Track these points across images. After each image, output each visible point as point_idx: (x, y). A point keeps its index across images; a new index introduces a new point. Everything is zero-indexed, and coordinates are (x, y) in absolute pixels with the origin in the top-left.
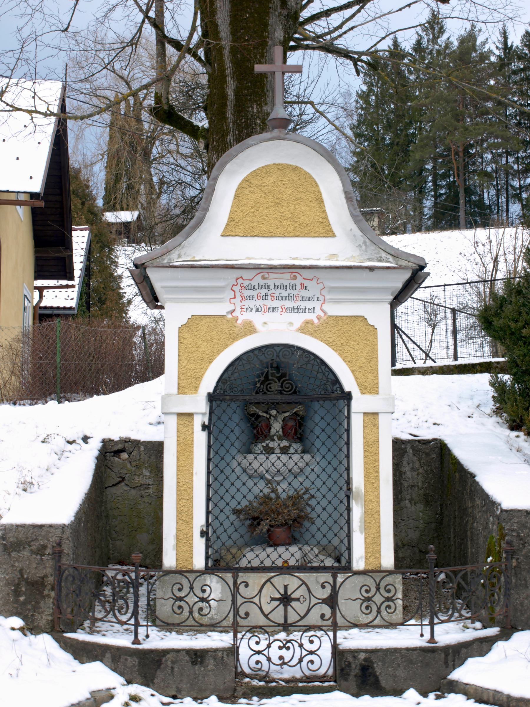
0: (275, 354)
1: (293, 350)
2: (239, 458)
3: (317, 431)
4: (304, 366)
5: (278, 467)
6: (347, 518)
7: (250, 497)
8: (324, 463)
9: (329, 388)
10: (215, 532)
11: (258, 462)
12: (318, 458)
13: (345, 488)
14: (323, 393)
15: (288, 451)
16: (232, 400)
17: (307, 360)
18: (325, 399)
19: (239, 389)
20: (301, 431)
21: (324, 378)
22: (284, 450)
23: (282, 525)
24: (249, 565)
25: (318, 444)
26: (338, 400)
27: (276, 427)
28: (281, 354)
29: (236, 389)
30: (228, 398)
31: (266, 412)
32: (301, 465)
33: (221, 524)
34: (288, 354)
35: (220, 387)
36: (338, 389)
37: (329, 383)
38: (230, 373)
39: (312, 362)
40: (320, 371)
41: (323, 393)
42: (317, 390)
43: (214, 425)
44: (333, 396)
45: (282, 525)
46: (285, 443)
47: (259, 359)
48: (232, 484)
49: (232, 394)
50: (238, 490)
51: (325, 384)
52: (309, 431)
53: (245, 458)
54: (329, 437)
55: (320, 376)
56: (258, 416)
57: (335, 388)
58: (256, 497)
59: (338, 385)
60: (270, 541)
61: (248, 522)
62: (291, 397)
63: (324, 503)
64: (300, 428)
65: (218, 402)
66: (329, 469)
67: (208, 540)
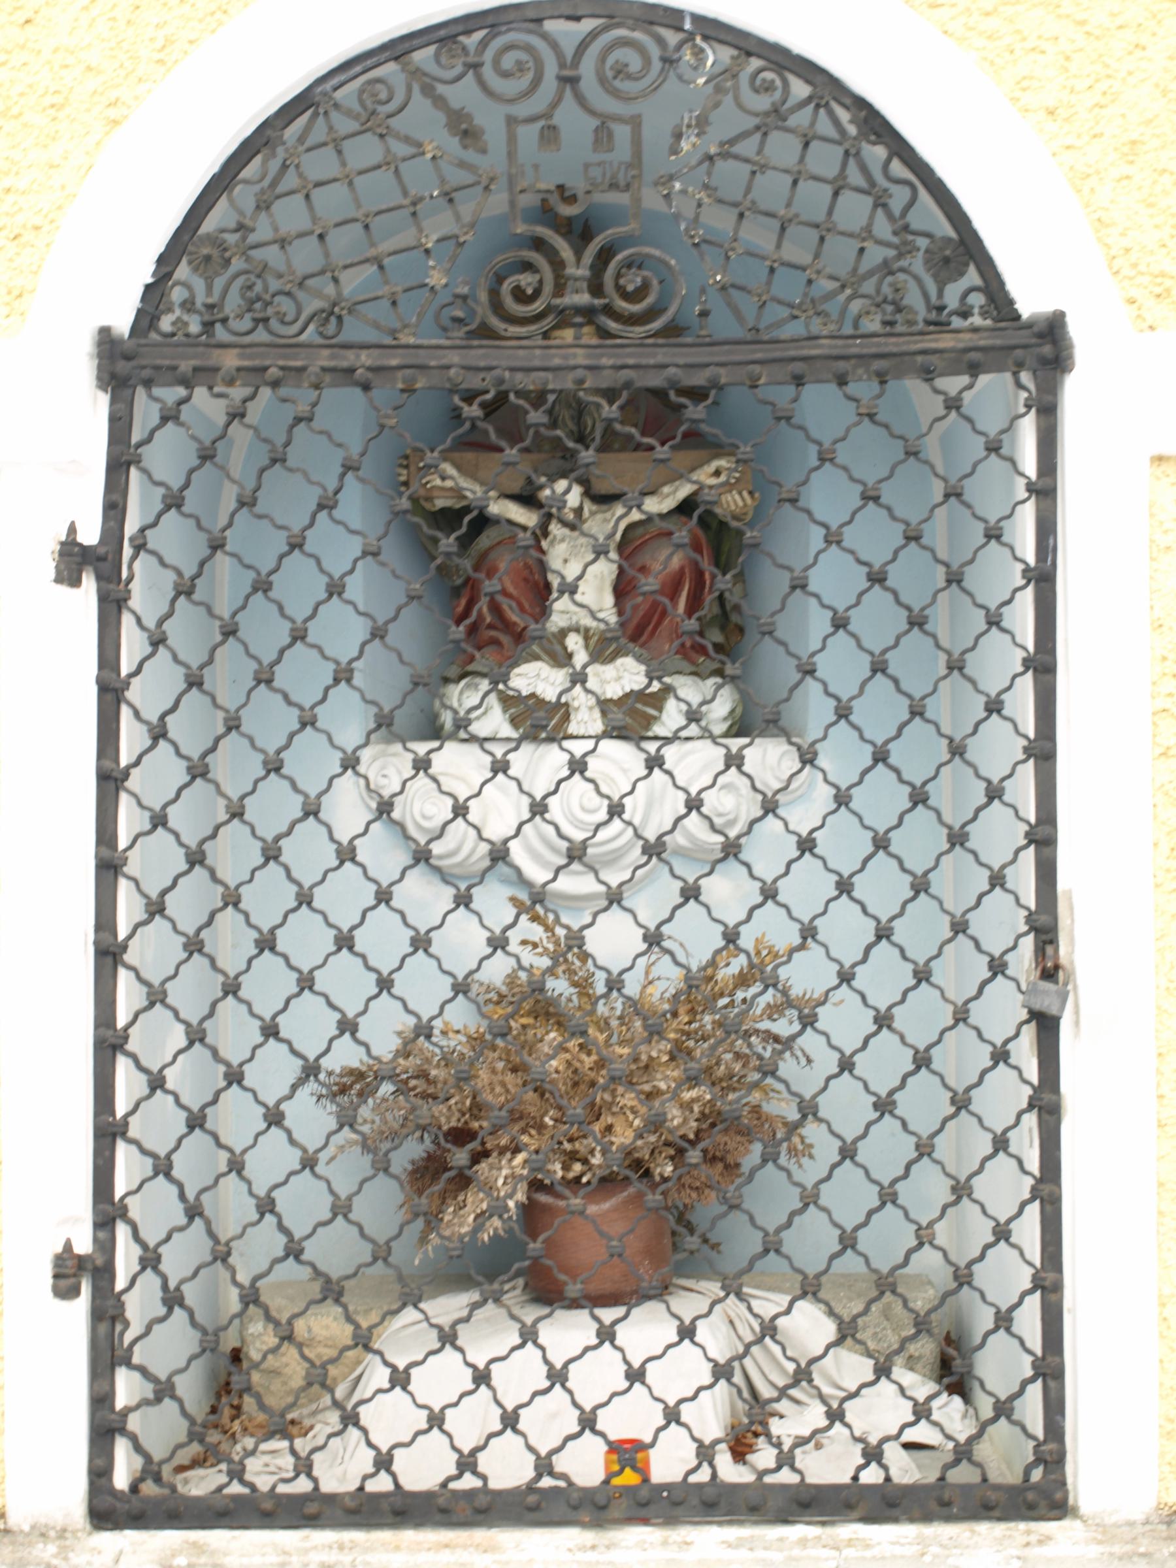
0: (551, 69)
1: (672, 38)
2: (388, 766)
3: (835, 579)
4: (742, 148)
5: (586, 824)
6: (1033, 1163)
7: (424, 988)
8: (881, 798)
9: (913, 299)
10: (150, 1260)
11: (478, 785)
12: (842, 756)
13: (1023, 960)
14: (872, 324)
15: (649, 721)
16: (255, 374)
17: (762, 103)
18: (888, 367)
19: (312, 305)
20: (724, 582)
21: (883, 228)
22: (629, 720)
23: (608, 1182)
24: (382, 1484)
25: (841, 665)
26: (974, 370)
27: (587, 586)
28: (587, 68)
29: (286, 305)
30: (230, 360)
31: (528, 499)
32: (731, 803)
33: (194, 1212)
34: (635, 63)
35: (177, 295)
36: (977, 300)
37: (917, 264)
38: (244, 195)
39: (801, 119)
40: (855, 177)
41: (872, 324)
42: (833, 307)
43: (140, 547)
44: (946, 342)
45: (608, 1182)
46: (625, 676)
47: (440, 102)
48: (266, 943)
49: (261, 335)
50: (306, 983)
51: (887, 269)
52: (785, 579)
53: (422, 765)
54: (917, 622)
55: (854, 210)
56: (483, 521)
57: (952, 296)
58: (461, 988)
59: (972, 277)
60: (534, 1270)
61: (412, 1150)
62: (661, 356)
63: (885, 1063)
64: (722, 563)
65: (171, 394)
66: (919, 840)
67: (107, 1313)
